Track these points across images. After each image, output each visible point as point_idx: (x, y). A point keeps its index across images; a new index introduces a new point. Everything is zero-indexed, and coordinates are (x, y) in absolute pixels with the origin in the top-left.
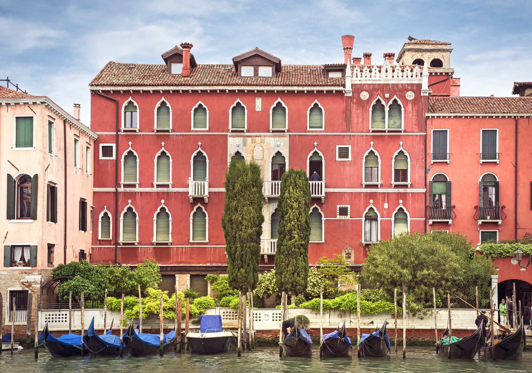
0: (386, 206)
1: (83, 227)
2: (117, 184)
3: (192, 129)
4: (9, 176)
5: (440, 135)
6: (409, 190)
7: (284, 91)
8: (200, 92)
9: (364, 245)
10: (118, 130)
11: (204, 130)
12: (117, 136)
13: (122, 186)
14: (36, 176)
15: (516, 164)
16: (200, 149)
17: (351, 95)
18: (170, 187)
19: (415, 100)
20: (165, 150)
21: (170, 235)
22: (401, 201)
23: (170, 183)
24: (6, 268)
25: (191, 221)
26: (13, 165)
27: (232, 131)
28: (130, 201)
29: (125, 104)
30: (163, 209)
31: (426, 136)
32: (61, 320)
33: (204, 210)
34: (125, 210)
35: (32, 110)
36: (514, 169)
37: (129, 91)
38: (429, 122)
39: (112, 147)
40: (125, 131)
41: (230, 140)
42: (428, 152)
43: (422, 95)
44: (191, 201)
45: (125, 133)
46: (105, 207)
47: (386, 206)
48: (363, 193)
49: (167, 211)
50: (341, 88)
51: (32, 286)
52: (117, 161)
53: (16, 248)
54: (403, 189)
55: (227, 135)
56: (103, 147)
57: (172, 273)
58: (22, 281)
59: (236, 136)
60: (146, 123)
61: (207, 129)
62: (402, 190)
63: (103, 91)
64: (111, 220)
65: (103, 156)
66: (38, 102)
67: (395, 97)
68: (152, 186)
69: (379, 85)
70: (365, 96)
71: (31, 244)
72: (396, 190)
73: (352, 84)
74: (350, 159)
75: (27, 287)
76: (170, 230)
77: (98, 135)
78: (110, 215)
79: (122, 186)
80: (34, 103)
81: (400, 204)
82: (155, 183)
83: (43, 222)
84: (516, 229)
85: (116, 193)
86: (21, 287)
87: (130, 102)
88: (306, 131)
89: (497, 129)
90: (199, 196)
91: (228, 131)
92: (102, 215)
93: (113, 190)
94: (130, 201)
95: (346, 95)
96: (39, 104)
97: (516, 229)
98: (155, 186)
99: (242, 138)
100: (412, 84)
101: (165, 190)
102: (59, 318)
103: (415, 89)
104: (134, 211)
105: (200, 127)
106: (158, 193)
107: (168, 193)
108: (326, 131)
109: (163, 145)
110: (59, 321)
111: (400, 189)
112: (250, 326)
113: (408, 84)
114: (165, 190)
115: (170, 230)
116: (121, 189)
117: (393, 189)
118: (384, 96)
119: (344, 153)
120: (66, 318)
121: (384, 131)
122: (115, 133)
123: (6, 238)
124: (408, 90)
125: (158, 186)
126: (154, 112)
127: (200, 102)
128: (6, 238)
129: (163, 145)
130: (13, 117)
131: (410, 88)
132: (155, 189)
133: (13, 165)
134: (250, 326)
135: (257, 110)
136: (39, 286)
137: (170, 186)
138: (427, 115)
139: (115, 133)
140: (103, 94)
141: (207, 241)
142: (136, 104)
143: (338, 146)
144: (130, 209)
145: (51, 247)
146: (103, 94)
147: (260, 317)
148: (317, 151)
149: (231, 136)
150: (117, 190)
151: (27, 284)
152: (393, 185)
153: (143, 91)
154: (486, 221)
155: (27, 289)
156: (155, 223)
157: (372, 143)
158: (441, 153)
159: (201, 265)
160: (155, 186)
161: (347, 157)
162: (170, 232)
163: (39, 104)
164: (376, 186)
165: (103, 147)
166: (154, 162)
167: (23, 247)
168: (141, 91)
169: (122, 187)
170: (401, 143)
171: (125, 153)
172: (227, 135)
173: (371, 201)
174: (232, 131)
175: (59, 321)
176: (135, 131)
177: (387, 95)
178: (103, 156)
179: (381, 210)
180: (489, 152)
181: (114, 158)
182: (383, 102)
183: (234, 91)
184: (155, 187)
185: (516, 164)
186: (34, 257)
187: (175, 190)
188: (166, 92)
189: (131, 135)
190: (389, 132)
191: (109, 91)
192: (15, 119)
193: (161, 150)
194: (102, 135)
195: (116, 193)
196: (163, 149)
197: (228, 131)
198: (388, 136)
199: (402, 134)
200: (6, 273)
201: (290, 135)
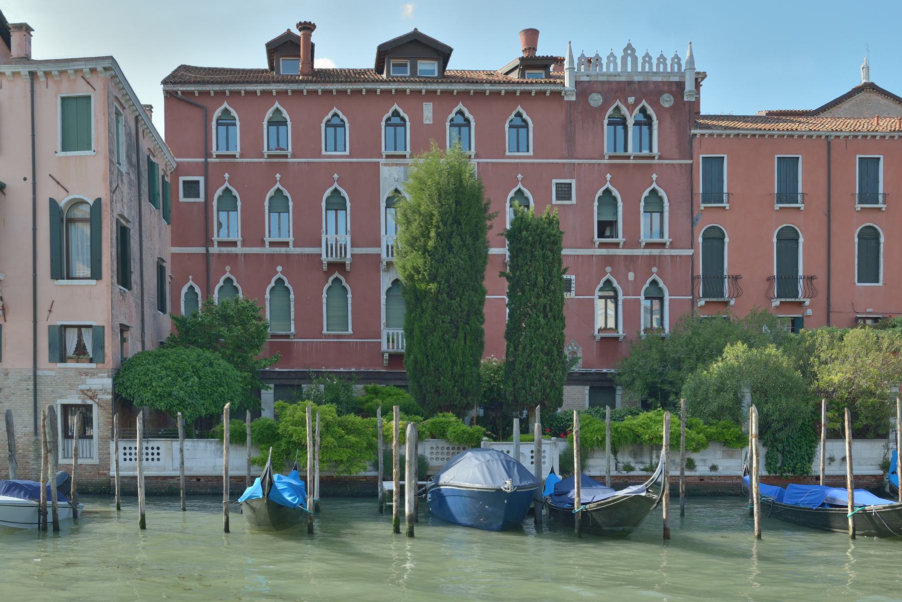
0: (631, 276)
1: (162, 307)
2: (208, 242)
3: (324, 152)
4: (53, 203)
5: (714, 165)
6: (667, 252)
7: (468, 92)
8: (334, 93)
9: (598, 338)
10: (208, 154)
11: (342, 155)
12: (206, 163)
13: (215, 243)
14: (98, 201)
15: (829, 211)
16: (336, 185)
17: (573, 98)
18: (291, 246)
19: (673, 108)
20: (281, 188)
21: (292, 322)
22: (654, 270)
23: (291, 239)
24: (53, 366)
25: (324, 301)
26: (58, 183)
27: (388, 157)
28: (228, 268)
29: (218, 113)
30: (280, 281)
31: (692, 164)
32: (150, 457)
33: (344, 283)
34: (221, 283)
35: (88, 83)
36: (825, 219)
37: (224, 92)
38: (696, 143)
39: (198, 182)
40: (218, 156)
41: (385, 171)
42: (695, 191)
43: (685, 99)
44: (325, 268)
45: (218, 160)
46: (191, 277)
47: (631, 276)
48: (597, 256)
49: (287, 284)
50: (558, 88)
51: (99, 397)
52: (207, 204)
53: (68, 330)
54: (659, 250)
55: (379, 163)
56: (184, 182)
57: (296, 382)
58: (81, 387)
59: (393, 165)
60: (252, 146)
61: (347, 152)
62: (656, 252)
63: (183, 92)
64: (200, 298)
65: (185, 196)
66: (100, 69)
67: (644, 103)
68: (262, 243)
69: (618, 82)
70: (596, 100)
71: (94, 323)
72: (647, 252)
73: (576, 82)
74: (574, 200)
75: (91, 398)
76: (292, 314)
77: (177, 163)
78: (198, 290)
79: (215, 243)
80: (93, 71)
81: (653, 274)
82: (267, 239)
83: (112, 284)
84: (829, 312)
85: (207, 255)
86: (79, 398)
87: (226, 111)
88: (504, 157)
89: (800, 156)
90: (338, 259)
91: (380, 156)
92: (185, 290)
93: (202, 250)
94: (228, 268)
95: (566, 99)
96: (101, 72)
97: (829, 312)
98: (267, 243)
99: (402, 168)
100: (670, 83)
101: (283, 250)
102: (153, 454)
103: (674, 89)
104: (235, 284)
105: (337, 152)
106: (271, 256)
107: (288, 256)
108: (535, 156)
109: (278, 179)
110: (153, 459)
111: (653, 250)
112: (46, 457)
113: (663, 82)
114: (283, 250)
115: (292, 314)
116: (215, 249)
117: (642, 250)
118: (626, 101)
119: (564, 192)
120: (125, 454)
121: (628, 158)
122: (203, 160)
123: (50, 311)
124: (661, 93)
125: (272, 244)
126: (262, 126)
127: (335, 110)
128: (50, 311)
129: (278, 179)
130: (56, 97)
131: (666, 88)
132: (267, 250)
133: (58, 183)
134: (46, 457)
135: (426, 122)
136: (110, 397)
137: (291, 244)
138: (693, 131)
139: (203, 160)
140: (184, 97)
141: (350, 331)
142: (234, 113)
143: (554, 181)
144: (228, 281)
145: (124, 328)
146: (184, 97)
147: (158, 454)
148: (522, 188)
149: (385, 165)
150: (207, 250)
151: (90, 394)
152: (644, 244)
153: (246, 92)
154: (798, 300)
155: (89, 402)
156: (268, 304)
157: (609, 176)
158: (713, 194)
159: (342, 370)
160: (267, 243)
161: (569, 198)
162: (292, 317)
163: (101, 72)
164: (616, 245)
165: (184, 182)
166: (264, 206)
167: (79, 327)
168: (243, 92)
169: (216, 246)
170: (654, 176)
171: (219, 192)
172: (379, 163)
173: (608, 269)
174: (388, 157)
175: (153, 459)
176: (234, 156)
177: (631, 100)
178: (185, 196)
179: (624, 282)
180: (787, 194)
181: (202, 199)
182: (625, 111)
183: (390, 91)
184: (267, 246)
185: (829, 211)
186: (99, 344)
187: (299, 250)
188: (282, 94)
189: (228, 163)
190: (635, 158)
191: (193, 93)
192: (59, 102)
193: (276, 187)
194: (183, 163)
195: (207, 255)
196: (278, 185)
197: (380, 156)
198: (633, 164)
199: (656, 161)
200: (53, 373)
201: (478, 163)
